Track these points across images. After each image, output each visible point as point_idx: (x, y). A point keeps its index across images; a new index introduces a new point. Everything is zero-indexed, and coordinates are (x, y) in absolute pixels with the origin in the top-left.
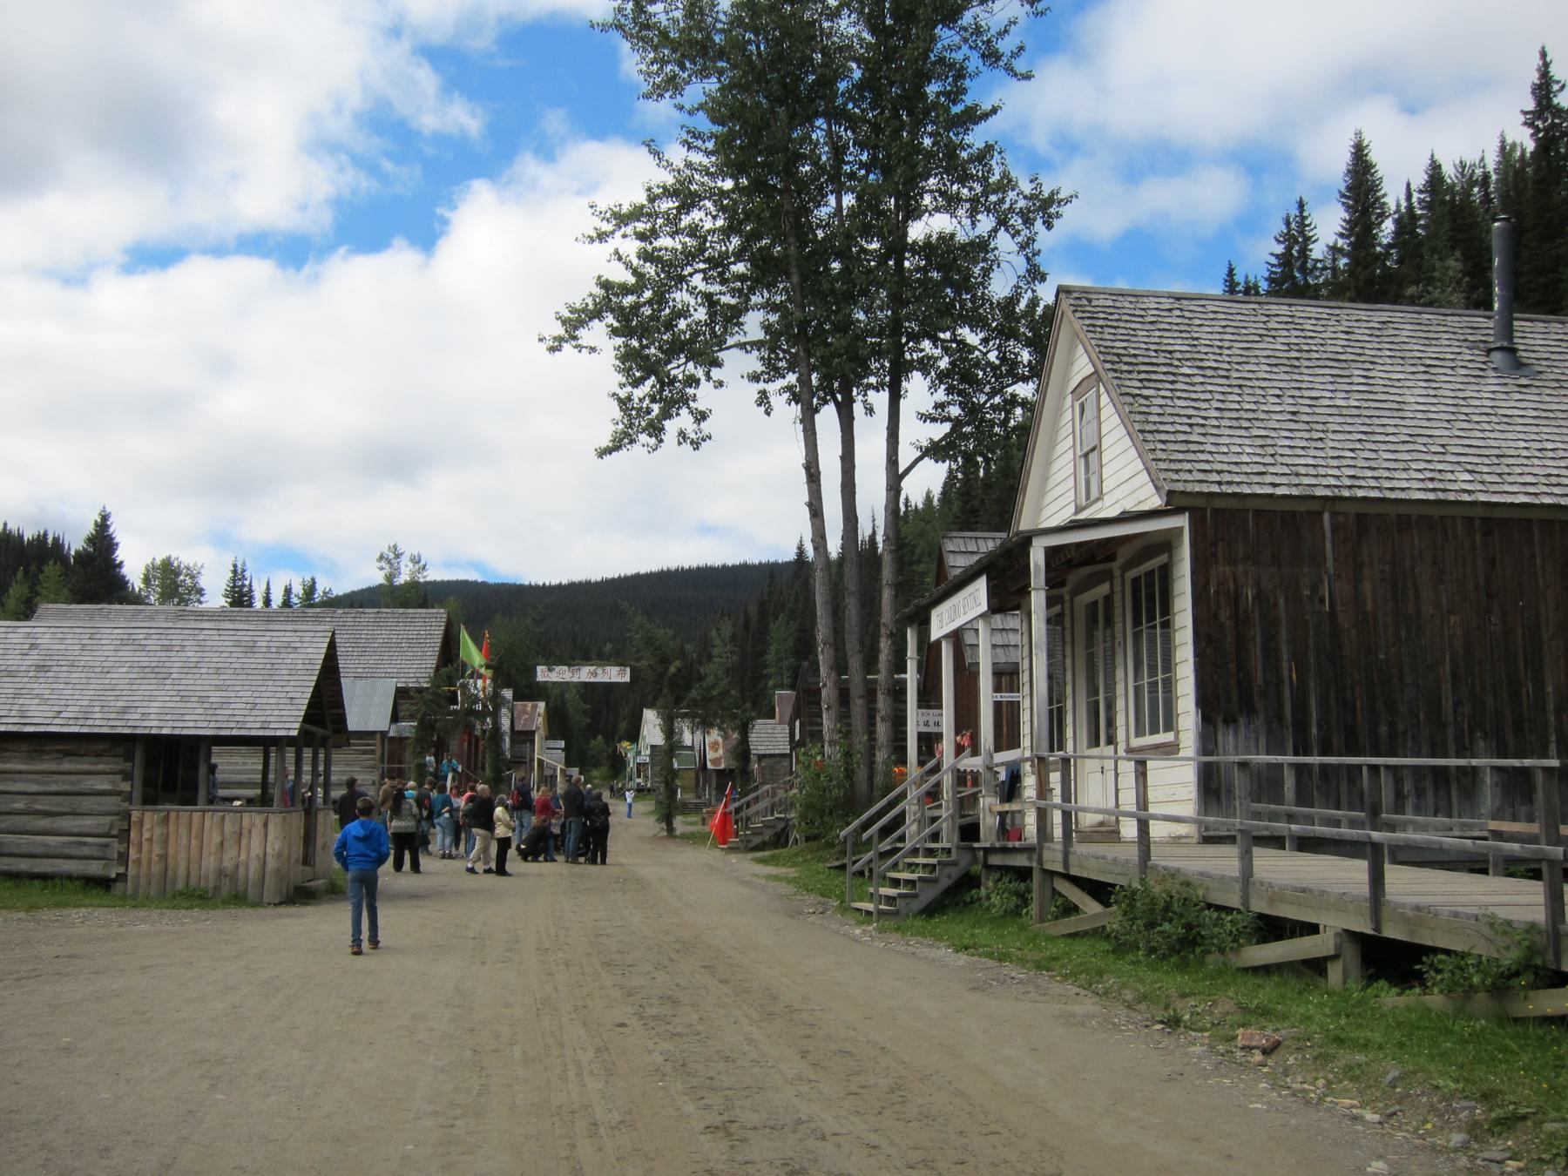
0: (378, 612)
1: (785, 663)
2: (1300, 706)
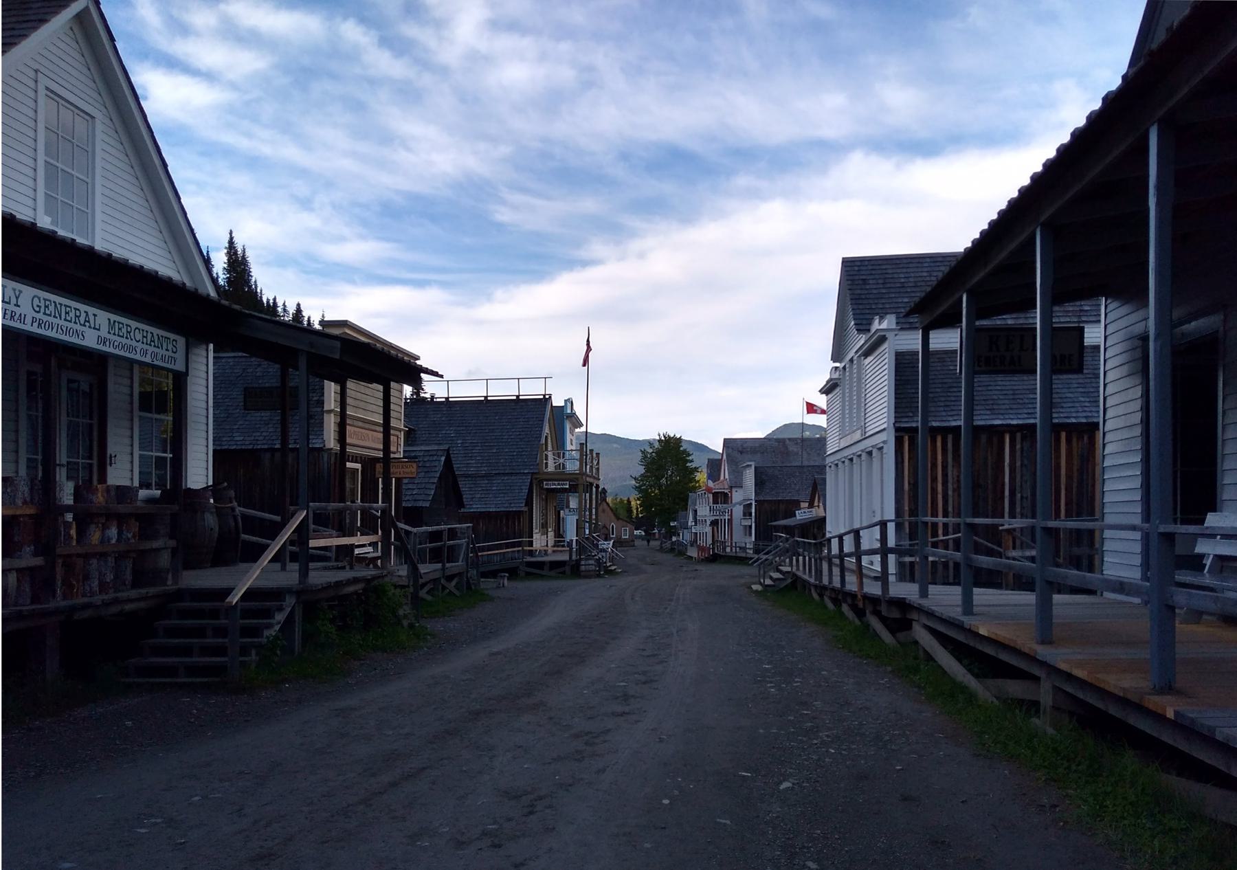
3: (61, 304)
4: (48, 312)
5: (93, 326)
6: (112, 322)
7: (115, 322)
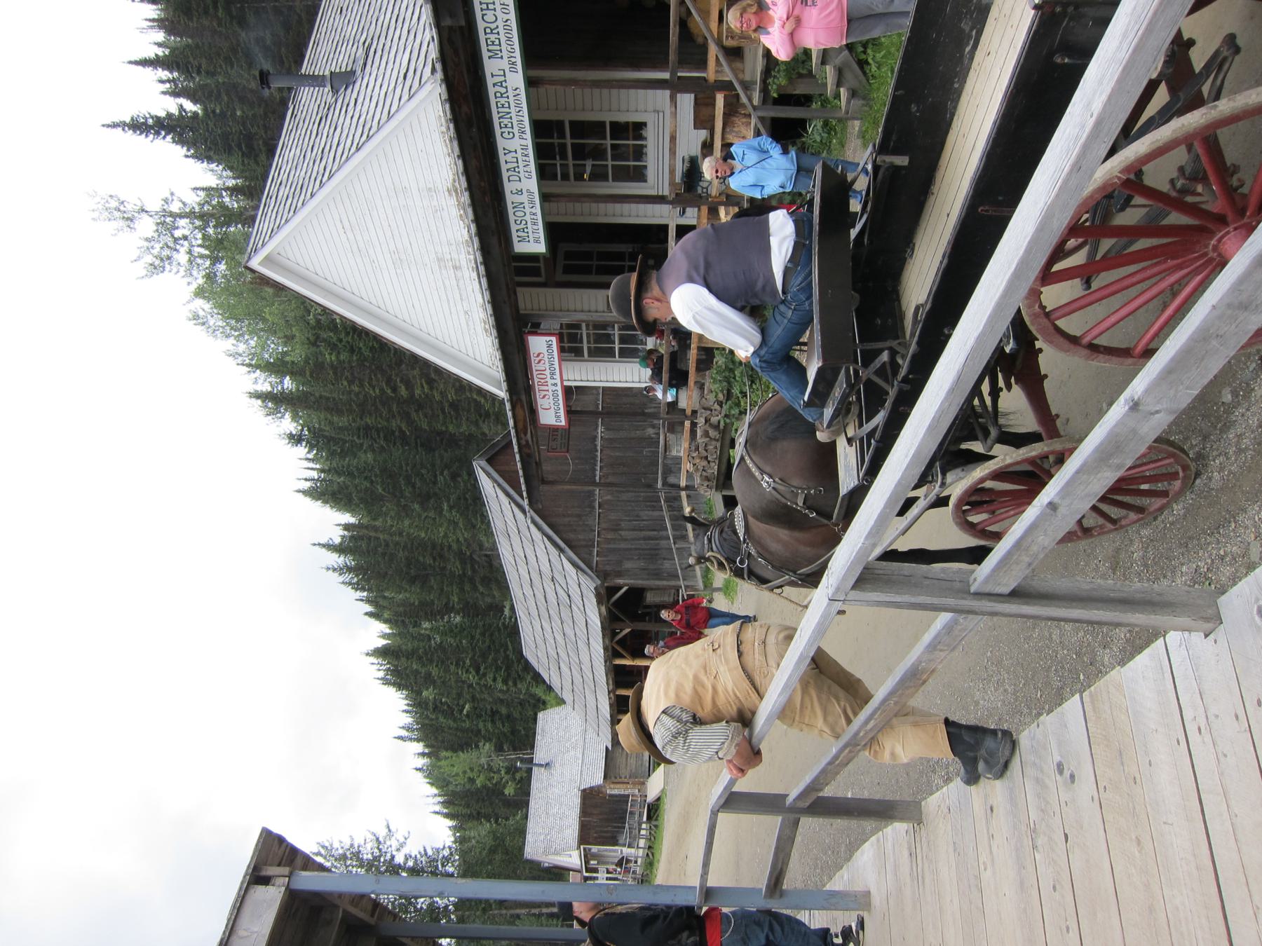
0: (1156, 68)
1: (544, 922)
2: (615, 827)
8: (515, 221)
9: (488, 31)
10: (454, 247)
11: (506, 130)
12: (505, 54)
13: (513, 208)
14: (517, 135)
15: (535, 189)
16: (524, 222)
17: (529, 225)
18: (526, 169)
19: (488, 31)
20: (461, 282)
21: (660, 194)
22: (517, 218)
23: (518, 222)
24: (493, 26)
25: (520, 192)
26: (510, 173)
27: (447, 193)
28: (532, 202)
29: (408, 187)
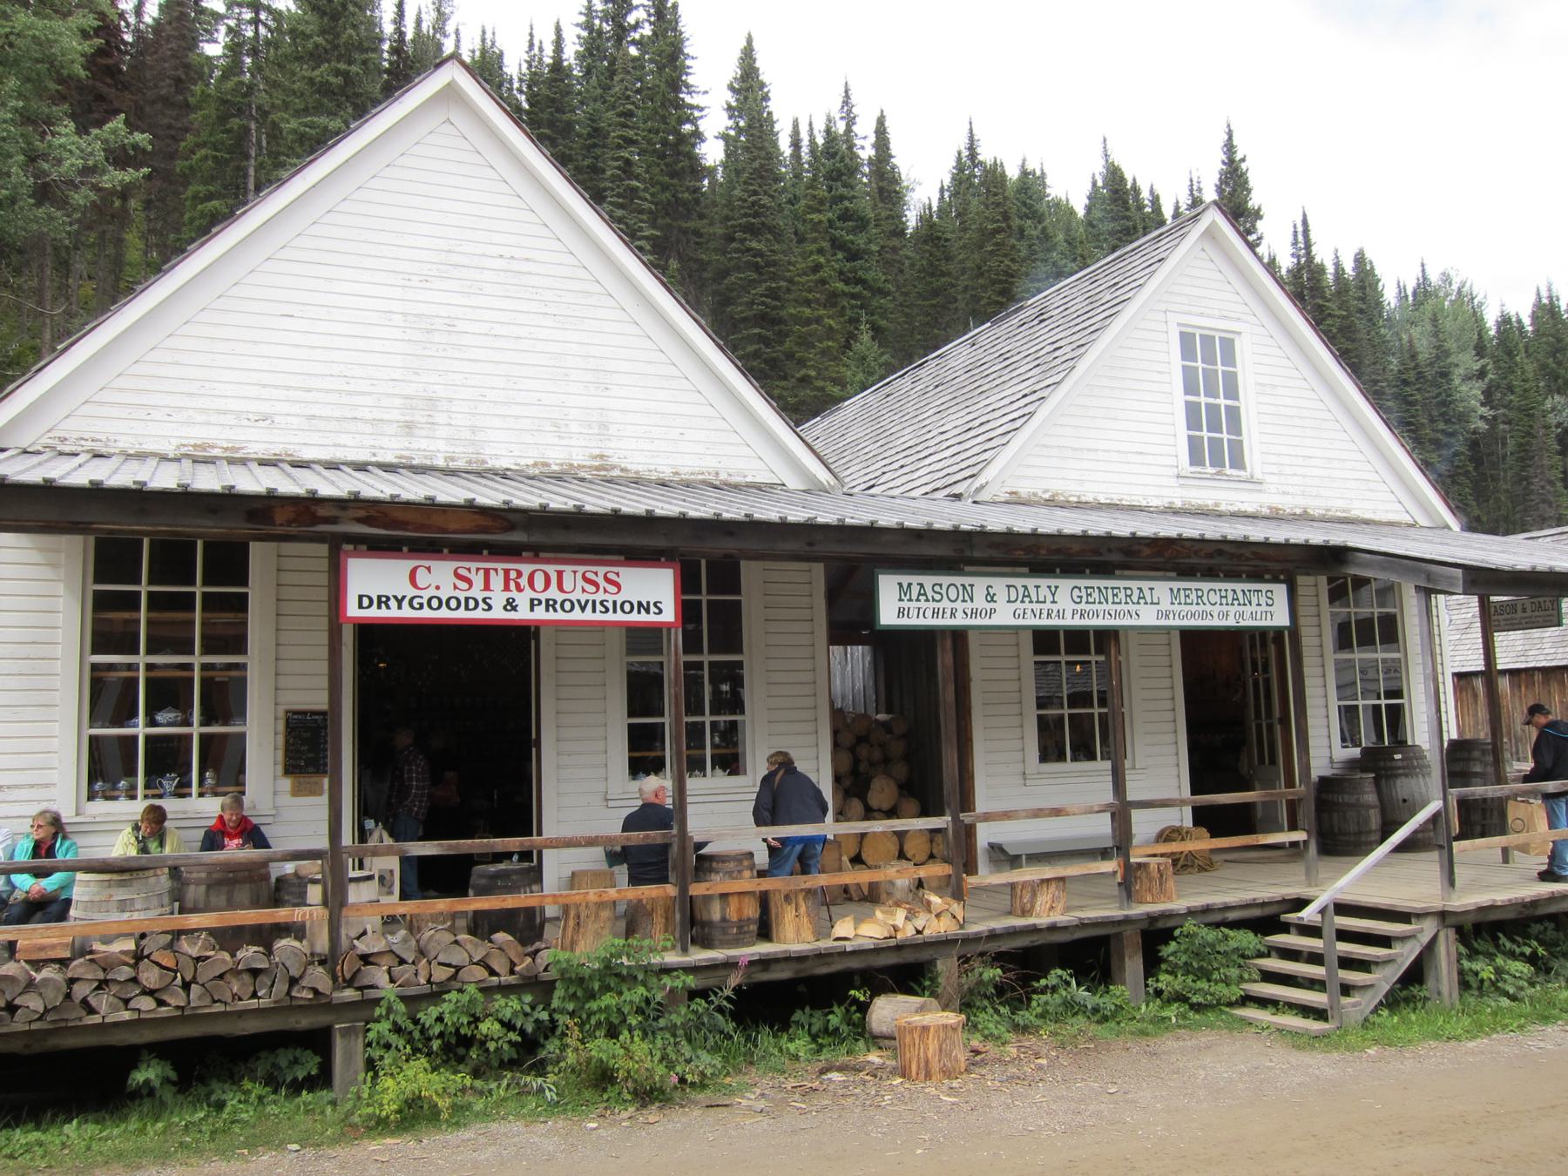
3: (1106, 588)
4: (1091, 600)
5: (1149, 601)
6: (905, 586)
7: (1179, 590)
8: (941, 585)
9: (1200, 593)
10: (466, 434)
11: (1084, 593)
12: (1177, 608)
13: (963, 585)
14: (1078, 607)
15: (996, 620)
16: (938, 597)
17: (932, 605)
18: (1029, 612)
19: (1200, 593)
20: (368, 428)
21: (689, 800)
22: (944, 587)
23: (937, 588)
24: (1205, 599)
25: (991, 598)
26: (1021, 590)
27: (597, 452)
28: (975, 613)
29: (607, 393)
